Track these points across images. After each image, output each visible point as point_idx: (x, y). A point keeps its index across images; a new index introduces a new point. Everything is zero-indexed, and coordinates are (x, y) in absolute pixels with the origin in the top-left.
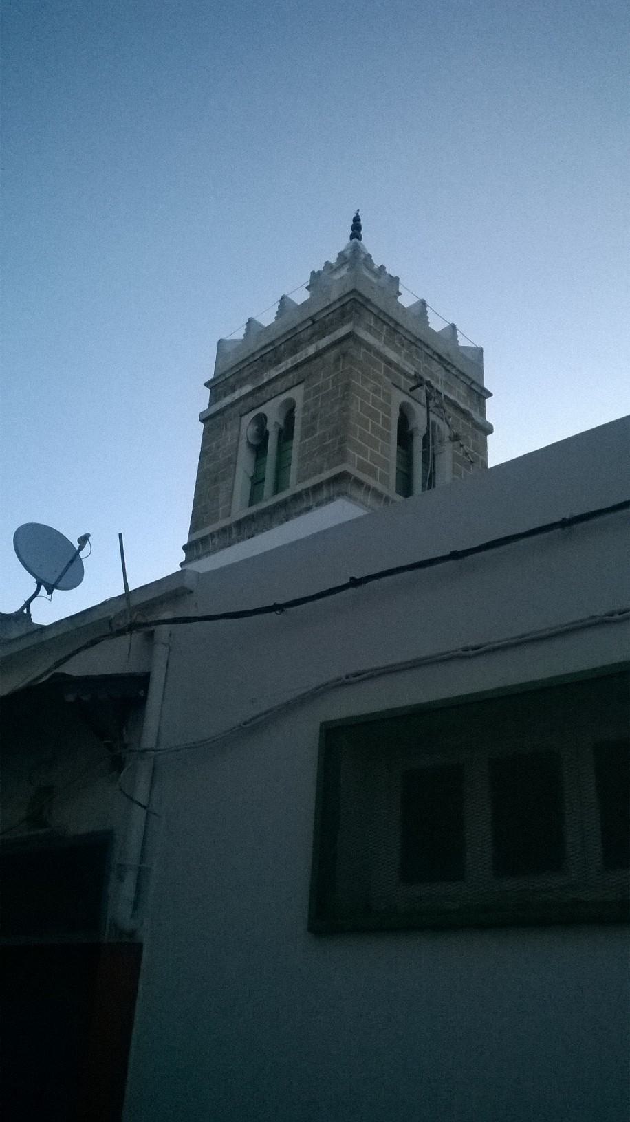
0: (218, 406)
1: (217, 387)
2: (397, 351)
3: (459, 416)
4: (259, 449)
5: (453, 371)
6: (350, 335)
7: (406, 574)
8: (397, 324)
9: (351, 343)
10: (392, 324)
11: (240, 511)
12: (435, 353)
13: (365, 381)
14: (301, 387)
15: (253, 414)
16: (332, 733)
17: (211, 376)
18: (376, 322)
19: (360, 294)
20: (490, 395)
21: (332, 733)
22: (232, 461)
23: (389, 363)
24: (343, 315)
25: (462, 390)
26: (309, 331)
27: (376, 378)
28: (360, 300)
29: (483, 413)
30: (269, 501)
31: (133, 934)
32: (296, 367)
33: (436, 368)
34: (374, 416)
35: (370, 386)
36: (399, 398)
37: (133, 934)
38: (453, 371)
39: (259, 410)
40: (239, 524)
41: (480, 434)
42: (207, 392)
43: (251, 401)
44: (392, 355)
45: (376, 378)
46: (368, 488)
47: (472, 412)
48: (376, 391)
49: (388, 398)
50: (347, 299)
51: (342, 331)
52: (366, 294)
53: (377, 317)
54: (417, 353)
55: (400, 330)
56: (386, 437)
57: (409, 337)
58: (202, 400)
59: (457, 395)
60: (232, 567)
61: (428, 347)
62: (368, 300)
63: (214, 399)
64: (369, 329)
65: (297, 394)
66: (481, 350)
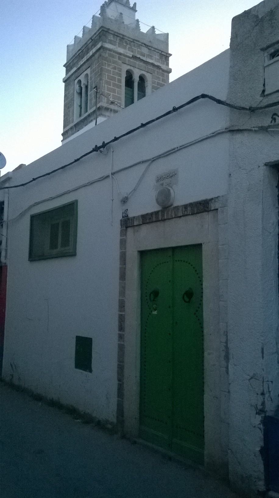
0: (70, 74)
1: (68, 66)
2: (125, 48)
3: (155, 69)
4: (80, 94)
5: (152, 49)
6: (102, 47)
7: (42, 178)
8: (123, 35)
9: (102, 50)
10: (121, 36)
11: (76, 120)
12: (142, 43)
13: (109, 65)
14: (89, 69)
15: (76, 81)
16: (33, 217)
17: (65, 62)
18: (113, 37)
19: (105, 28)
20: (171, 55)
21: (33, 217)
22: (73, 100)
23: (120, 54)
24: (100, 37)
25: (157, 57)
26: (91, 44)
27: (114, 62)
28: (106, 30)
29: (168, 64)
30: (84, 115)
31: (5, 263)
32: (88, 60)
33: (145, 50)
34: (114, 79)
35: (111, 67)
36: (125, 68)
37: (5, 263)
38: (152, 49)
39: (79, 78)
40: (76, 126)
41: (165, 74)
42: (65, 69)
43: (76, 74)
44: (121, 50)
45: (114, 62)
46: (111, 110)
47: (161, 65)
48: (115, 68)
49: (120, 70)
50: (100, 30)
51: (99, 46)
52: (107, 27)
53: (114, 35)
54: (134, 45)
55: (125, 38)
56: (119, 87)
57: (130, 40)
58: (62, 73)
59: (154, 60)
60: (71, 140)
61: (138, 41)
62: (109, 29)
63: (67, 72)
64: (111, 42)
65: (88, 71)
66: (168, 34)
